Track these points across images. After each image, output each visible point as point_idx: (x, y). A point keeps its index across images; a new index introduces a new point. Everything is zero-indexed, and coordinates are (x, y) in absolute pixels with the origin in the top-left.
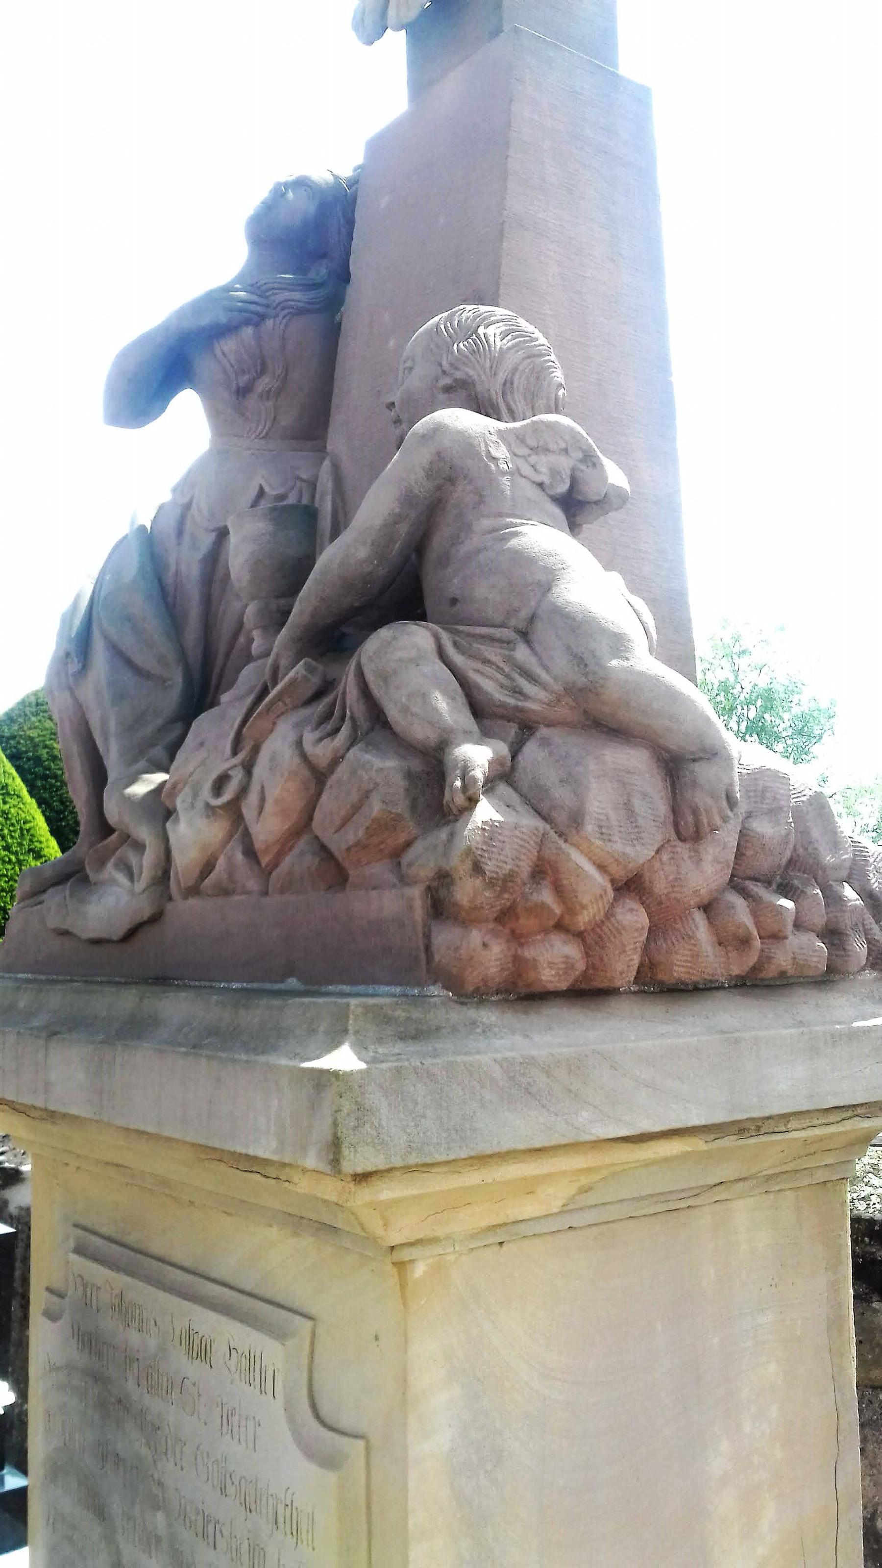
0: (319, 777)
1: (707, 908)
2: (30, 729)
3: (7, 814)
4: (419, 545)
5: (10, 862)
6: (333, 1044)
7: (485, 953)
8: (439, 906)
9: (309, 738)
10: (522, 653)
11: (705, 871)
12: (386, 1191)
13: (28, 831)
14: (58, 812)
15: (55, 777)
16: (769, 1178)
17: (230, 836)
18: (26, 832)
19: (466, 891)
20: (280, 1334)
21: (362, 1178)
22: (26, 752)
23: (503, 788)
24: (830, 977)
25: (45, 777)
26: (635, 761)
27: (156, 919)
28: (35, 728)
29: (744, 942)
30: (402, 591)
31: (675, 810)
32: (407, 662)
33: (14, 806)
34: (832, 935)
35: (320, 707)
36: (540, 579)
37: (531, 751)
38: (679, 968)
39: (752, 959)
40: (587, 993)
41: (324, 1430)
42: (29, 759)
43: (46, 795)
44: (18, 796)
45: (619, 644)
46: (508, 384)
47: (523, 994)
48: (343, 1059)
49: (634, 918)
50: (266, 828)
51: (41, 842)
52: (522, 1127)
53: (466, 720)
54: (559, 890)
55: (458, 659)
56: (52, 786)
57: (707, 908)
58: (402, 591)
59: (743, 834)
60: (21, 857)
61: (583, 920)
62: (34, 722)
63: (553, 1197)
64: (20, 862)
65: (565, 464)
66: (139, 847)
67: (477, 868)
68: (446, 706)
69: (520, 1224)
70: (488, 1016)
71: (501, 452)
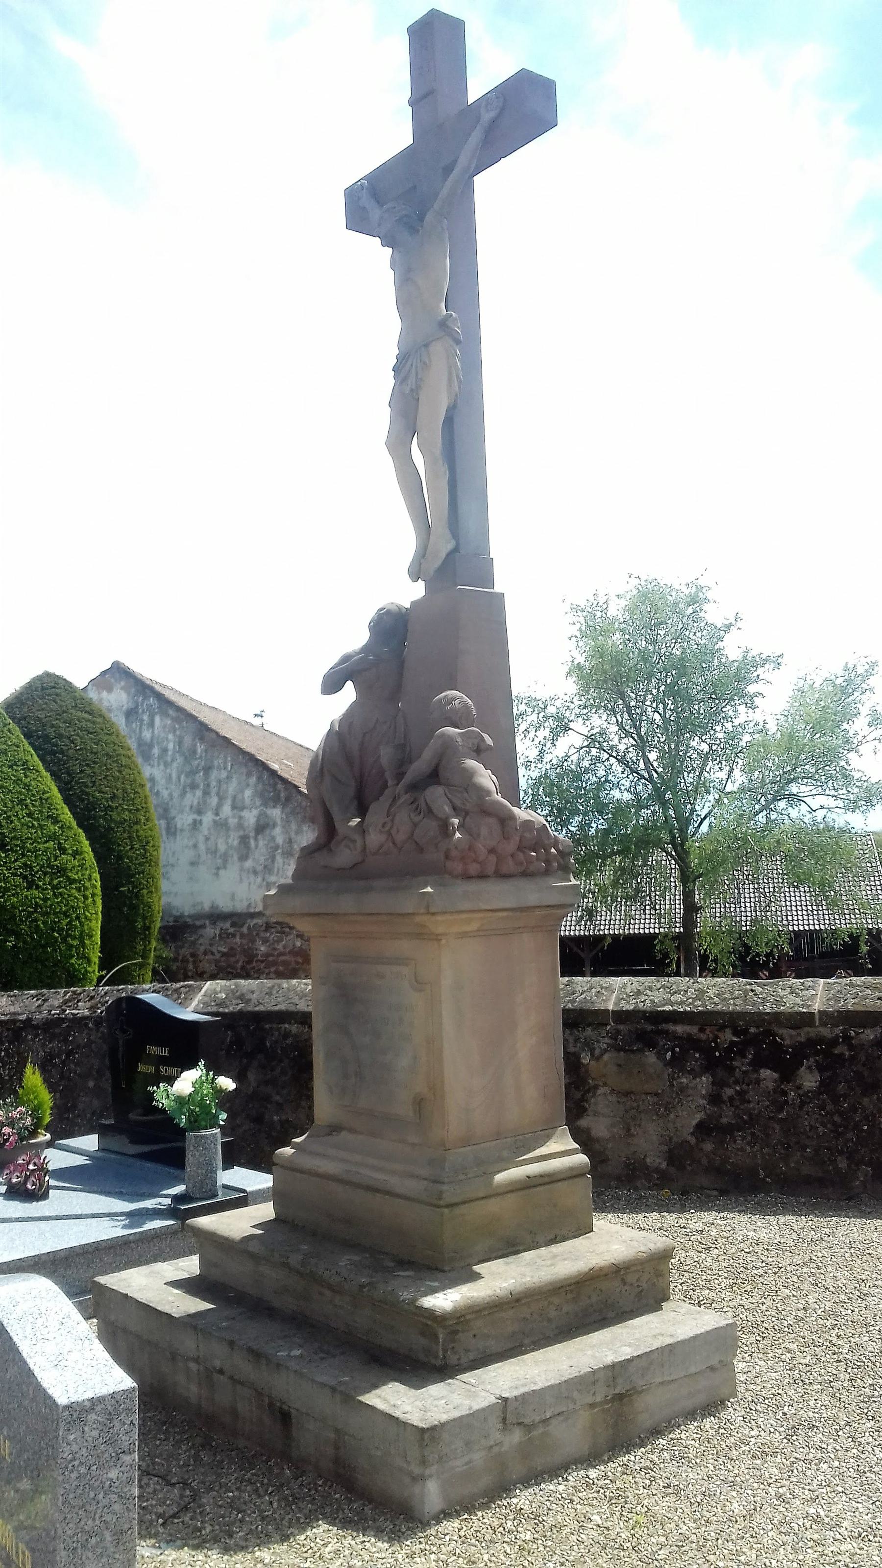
0: (415, 825)
1: (512, 856)
2: (38, 710)
3: (29, 786)
4: (437, 766)
5: (33, 826)
6: (426, 887)
7: (458, 867)
8: (447, 857)
9: (412, 815)
10: (465, 795)
11: (511, 847)
12: (439, 918)
13: (46, 800)
14: (66, 783)
15: (62, 752)
16: (533, 928)
17: (387, 839)
18: (45, 801)
19: (454, 853)
20: (407, 965)
21: (433, 914)
22: (37, 731)
23: (462, 829)
24: (547, 872)
25: (54, 753)
26: (492, 821)
27: (363, 861)
28: (43, 710)
29: (522, 863)
30: (434, 776)
31: (503, 833)
32: (436, 795)
33: (34, 779)
34: (548, 862)
35: (414, 806)
36: (470, 774)
37: (468, 819)
38: (504, 870)
39: (523, 868)
40: (482, 876)
41: (419, 984)
42: (39, 738)
43: (55, 769)
44: (37, 771)
45: (488, 793)
46: (460, 718)
47: (467, 877)
48: (429, 889)
49: (493, 858)
50: (400, 837)
51: (57, 810)
52: (467, 906)
53: (453, 813)
54: (475, 852)
55: (450, 796)
56: (60, 760)
57: (512, 856)
58: (434, 776)
59: (521, 837)
60: (42, 823)
61: (481, 859)
62: (41, 705)
63: (474, 926)
64: (41, 827)
65: (476, 741)
66: (354, 841)
67: (456, 848)
68: (447, 809)
69: (472, 1204)
70: (459, 881)
71: (459, 740)
